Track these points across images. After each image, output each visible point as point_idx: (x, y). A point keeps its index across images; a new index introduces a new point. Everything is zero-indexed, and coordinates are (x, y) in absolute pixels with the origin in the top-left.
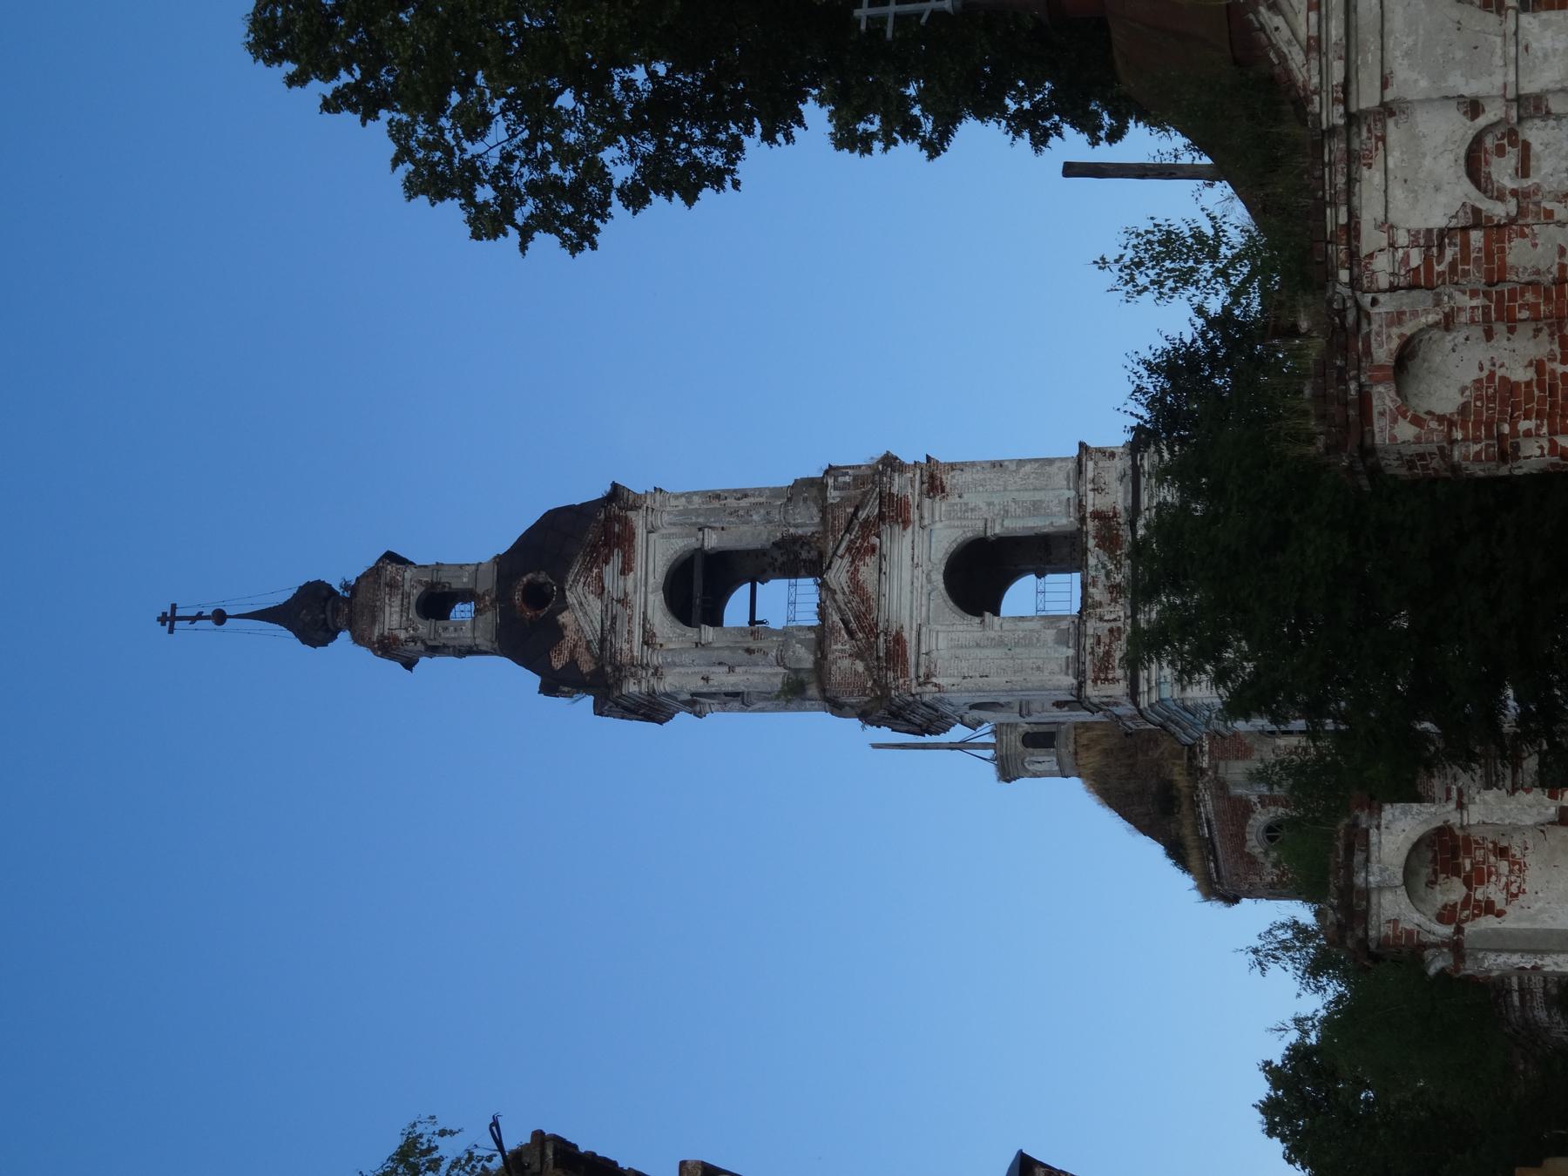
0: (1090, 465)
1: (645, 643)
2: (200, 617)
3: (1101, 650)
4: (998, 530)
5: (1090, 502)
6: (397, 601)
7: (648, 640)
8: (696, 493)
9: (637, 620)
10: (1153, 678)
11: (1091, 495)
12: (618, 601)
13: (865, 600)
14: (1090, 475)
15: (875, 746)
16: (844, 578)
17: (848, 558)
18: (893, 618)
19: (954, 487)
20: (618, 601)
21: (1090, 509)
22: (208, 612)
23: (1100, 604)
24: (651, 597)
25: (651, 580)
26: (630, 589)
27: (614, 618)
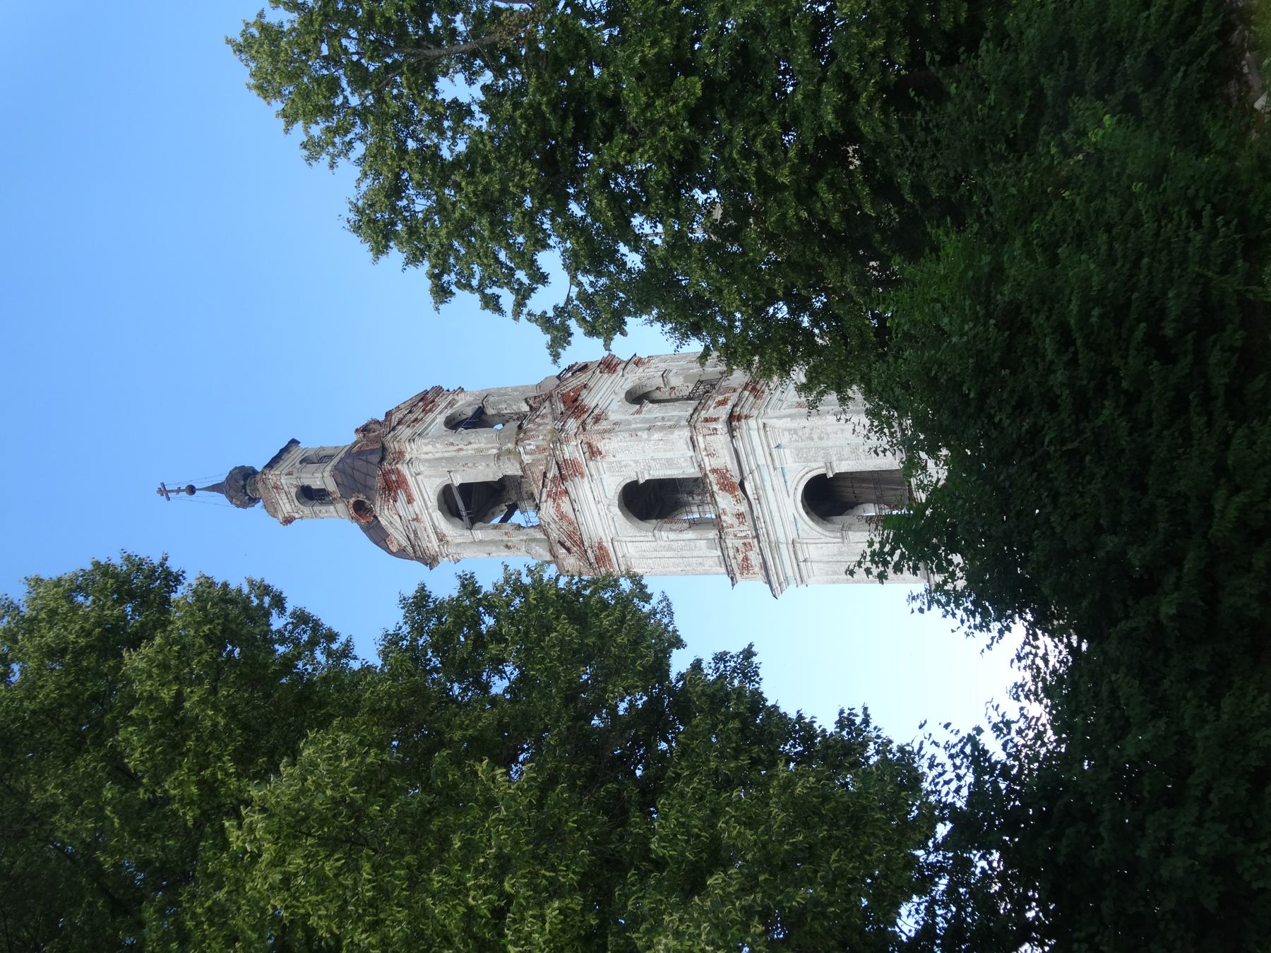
0: (700, 439)
2: (179, 490)
3: (741, 557)
4: (647, 478)
5: (707, 464)
6: (283, 496)
7: (441, 538)
8: (391, 553)
10: (1180, 74)
11: (706, 459)
13: (571, 523)
14: (702, 446)
16: (552, 511)
17: (550, 501)
18: (593, 535)
19: (607, 451)
21: (708, 468)
22: (183, 487)
23: (732, 526)
24: (434, 515)
27: (415, 532)
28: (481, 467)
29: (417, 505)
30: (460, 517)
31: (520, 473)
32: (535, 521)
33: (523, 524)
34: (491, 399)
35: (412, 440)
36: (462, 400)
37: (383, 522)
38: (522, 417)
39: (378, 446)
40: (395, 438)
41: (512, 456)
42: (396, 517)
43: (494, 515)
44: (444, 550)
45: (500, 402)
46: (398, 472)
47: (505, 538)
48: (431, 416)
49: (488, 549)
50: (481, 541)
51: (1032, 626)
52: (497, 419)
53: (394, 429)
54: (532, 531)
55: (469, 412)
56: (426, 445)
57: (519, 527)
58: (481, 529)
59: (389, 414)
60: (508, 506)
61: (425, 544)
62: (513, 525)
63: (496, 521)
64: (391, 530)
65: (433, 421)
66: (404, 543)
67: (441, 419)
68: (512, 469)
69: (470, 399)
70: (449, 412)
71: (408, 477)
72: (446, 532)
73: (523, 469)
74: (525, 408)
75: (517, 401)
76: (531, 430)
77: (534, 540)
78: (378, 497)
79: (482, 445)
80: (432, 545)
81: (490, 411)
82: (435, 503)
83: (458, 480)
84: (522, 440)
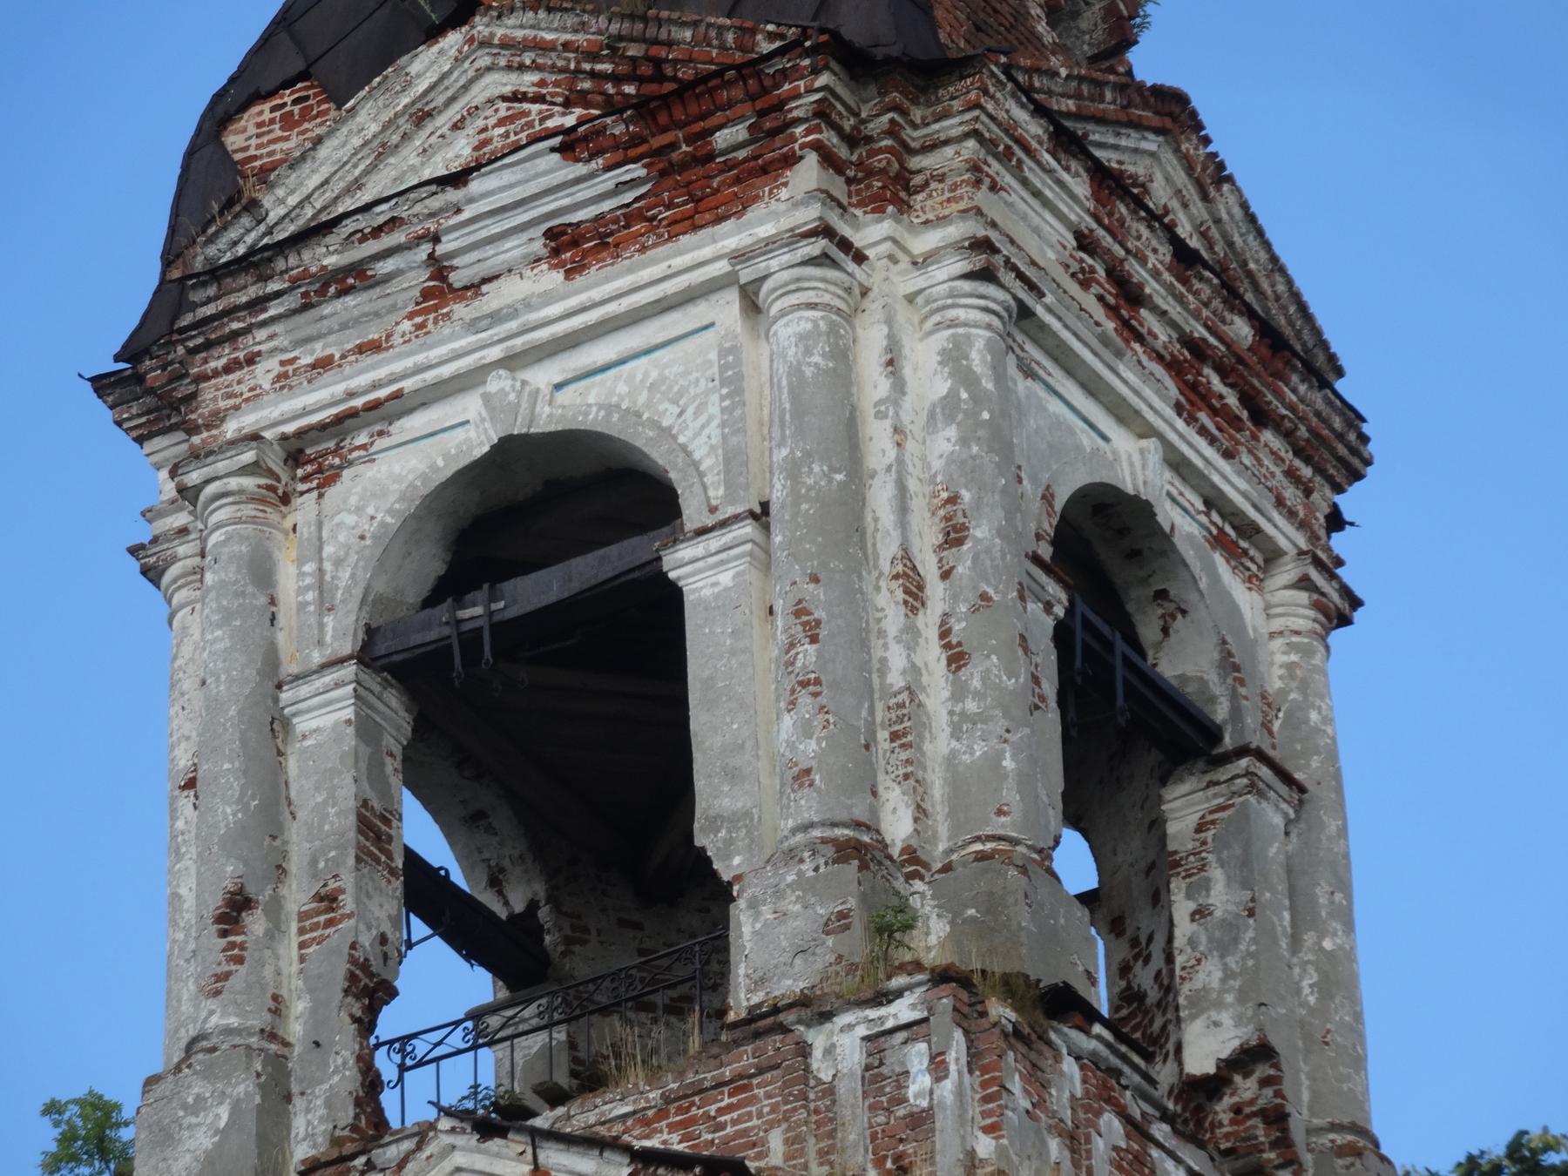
1: (296, 450)
7: (310, 457)
8: (223, 111)
9: (363, 379)
12: (439, 268)
15: (712, 325)
20: (439, 268)
24: (470, 406)
25: (543, 376)
26: (497, 296)
28: (791, 734)
29: (539, 294)
30: (449, 588)
31: (743, 997)
32: (410, 1101)
33: (391, 1023)
34: (1271, 814)
35: (987, 260)
36: (1267, 612)
37: (427, 65)
38: (1145, 1023)
39: (953, 35)
40: (1006, 148)
41: (857, 943)
42: (460, 150)
43: (460, 821)
44: (227, 475)
45: (1245, 873)
46: (765, 167)
47: (297, 895)
48: (1155, 397)
49: (225, 772)
50: (278, 726)
51: (118, 1125)
52: (1134, 849)
53: (1067, 142)
54: (341, 1076)
55: (1183, 661)
56: (954, 358)
57: (371, 990)
58: (366, 728)
59: (1172, 112)
60: (526, 922)
61: (274, 342)
62: (393, 950)
63: (422, 833)
64: (369, 115)
65: (1124, 414)
66: (284, 203)
67: (1134, 465)
68: (771, 943)
69: (1275, 664)
70: (1183, 522)
71: (729, 237)
72: (352, 486)
73: (765, 1022)
74: (1205, 1046)
75: (1253, 994)
76: (1038, 1080)
77: (278, 1094)
78: (599, 28)
79: (939, 744)
80: (266, 399)
81: (1185, 807)
82: (547, 418)
83: (705, 572)
84: (969, 1016)
